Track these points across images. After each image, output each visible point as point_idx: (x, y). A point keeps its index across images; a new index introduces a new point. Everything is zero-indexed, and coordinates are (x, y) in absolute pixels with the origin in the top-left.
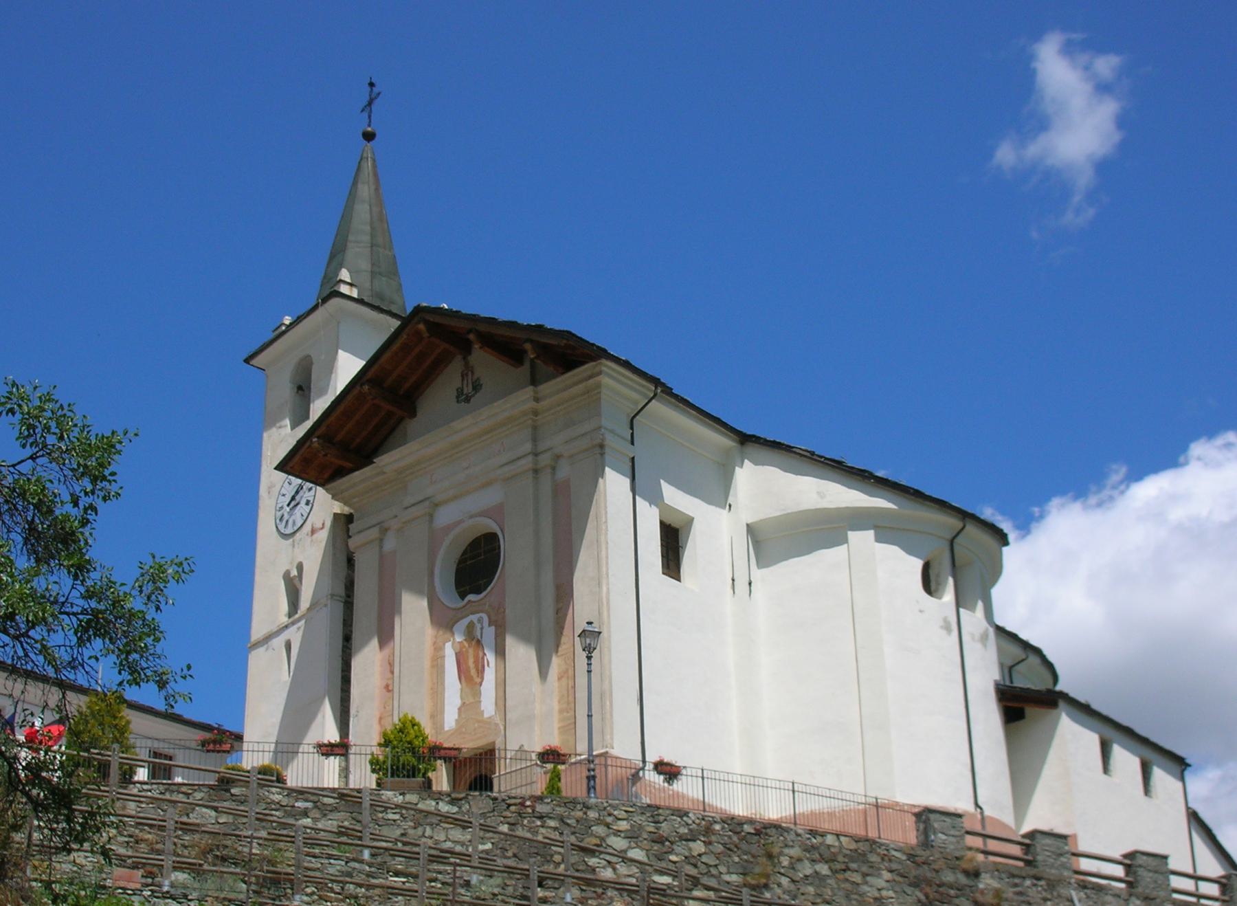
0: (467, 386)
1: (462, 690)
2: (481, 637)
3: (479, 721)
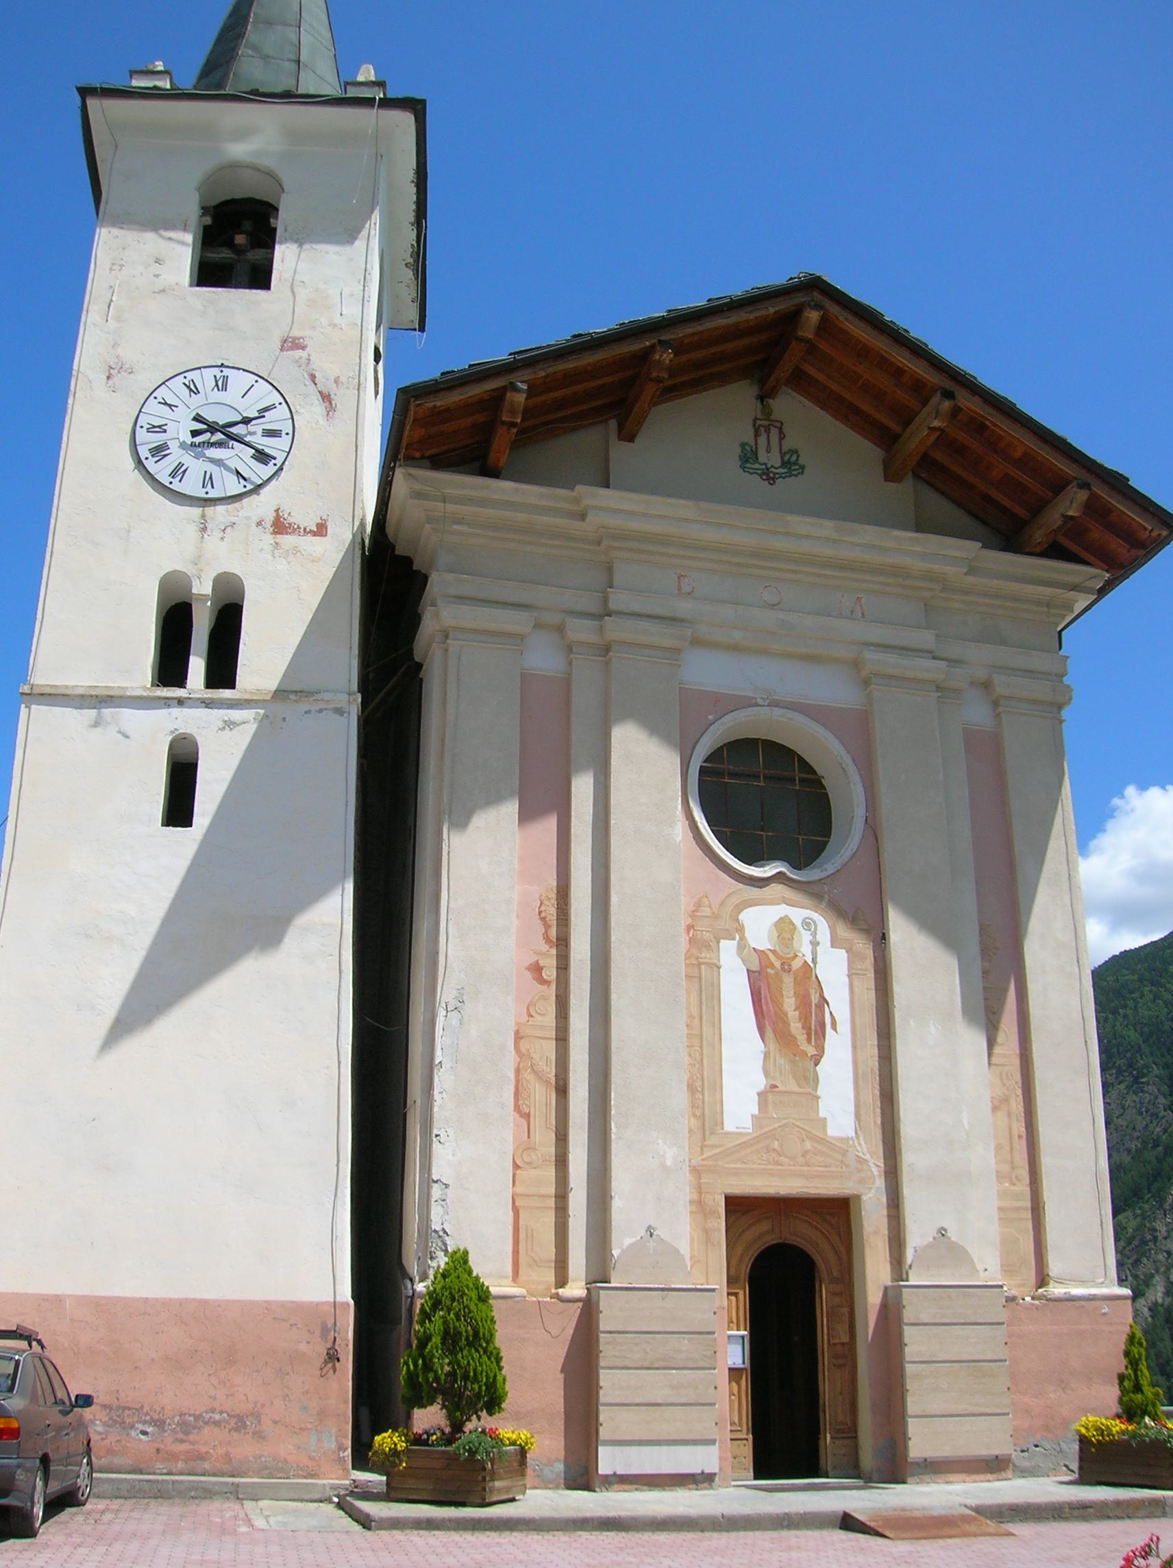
0: (768, 451)
1: (766, 1055)
2: (814, 960)
3: (813, 1138)
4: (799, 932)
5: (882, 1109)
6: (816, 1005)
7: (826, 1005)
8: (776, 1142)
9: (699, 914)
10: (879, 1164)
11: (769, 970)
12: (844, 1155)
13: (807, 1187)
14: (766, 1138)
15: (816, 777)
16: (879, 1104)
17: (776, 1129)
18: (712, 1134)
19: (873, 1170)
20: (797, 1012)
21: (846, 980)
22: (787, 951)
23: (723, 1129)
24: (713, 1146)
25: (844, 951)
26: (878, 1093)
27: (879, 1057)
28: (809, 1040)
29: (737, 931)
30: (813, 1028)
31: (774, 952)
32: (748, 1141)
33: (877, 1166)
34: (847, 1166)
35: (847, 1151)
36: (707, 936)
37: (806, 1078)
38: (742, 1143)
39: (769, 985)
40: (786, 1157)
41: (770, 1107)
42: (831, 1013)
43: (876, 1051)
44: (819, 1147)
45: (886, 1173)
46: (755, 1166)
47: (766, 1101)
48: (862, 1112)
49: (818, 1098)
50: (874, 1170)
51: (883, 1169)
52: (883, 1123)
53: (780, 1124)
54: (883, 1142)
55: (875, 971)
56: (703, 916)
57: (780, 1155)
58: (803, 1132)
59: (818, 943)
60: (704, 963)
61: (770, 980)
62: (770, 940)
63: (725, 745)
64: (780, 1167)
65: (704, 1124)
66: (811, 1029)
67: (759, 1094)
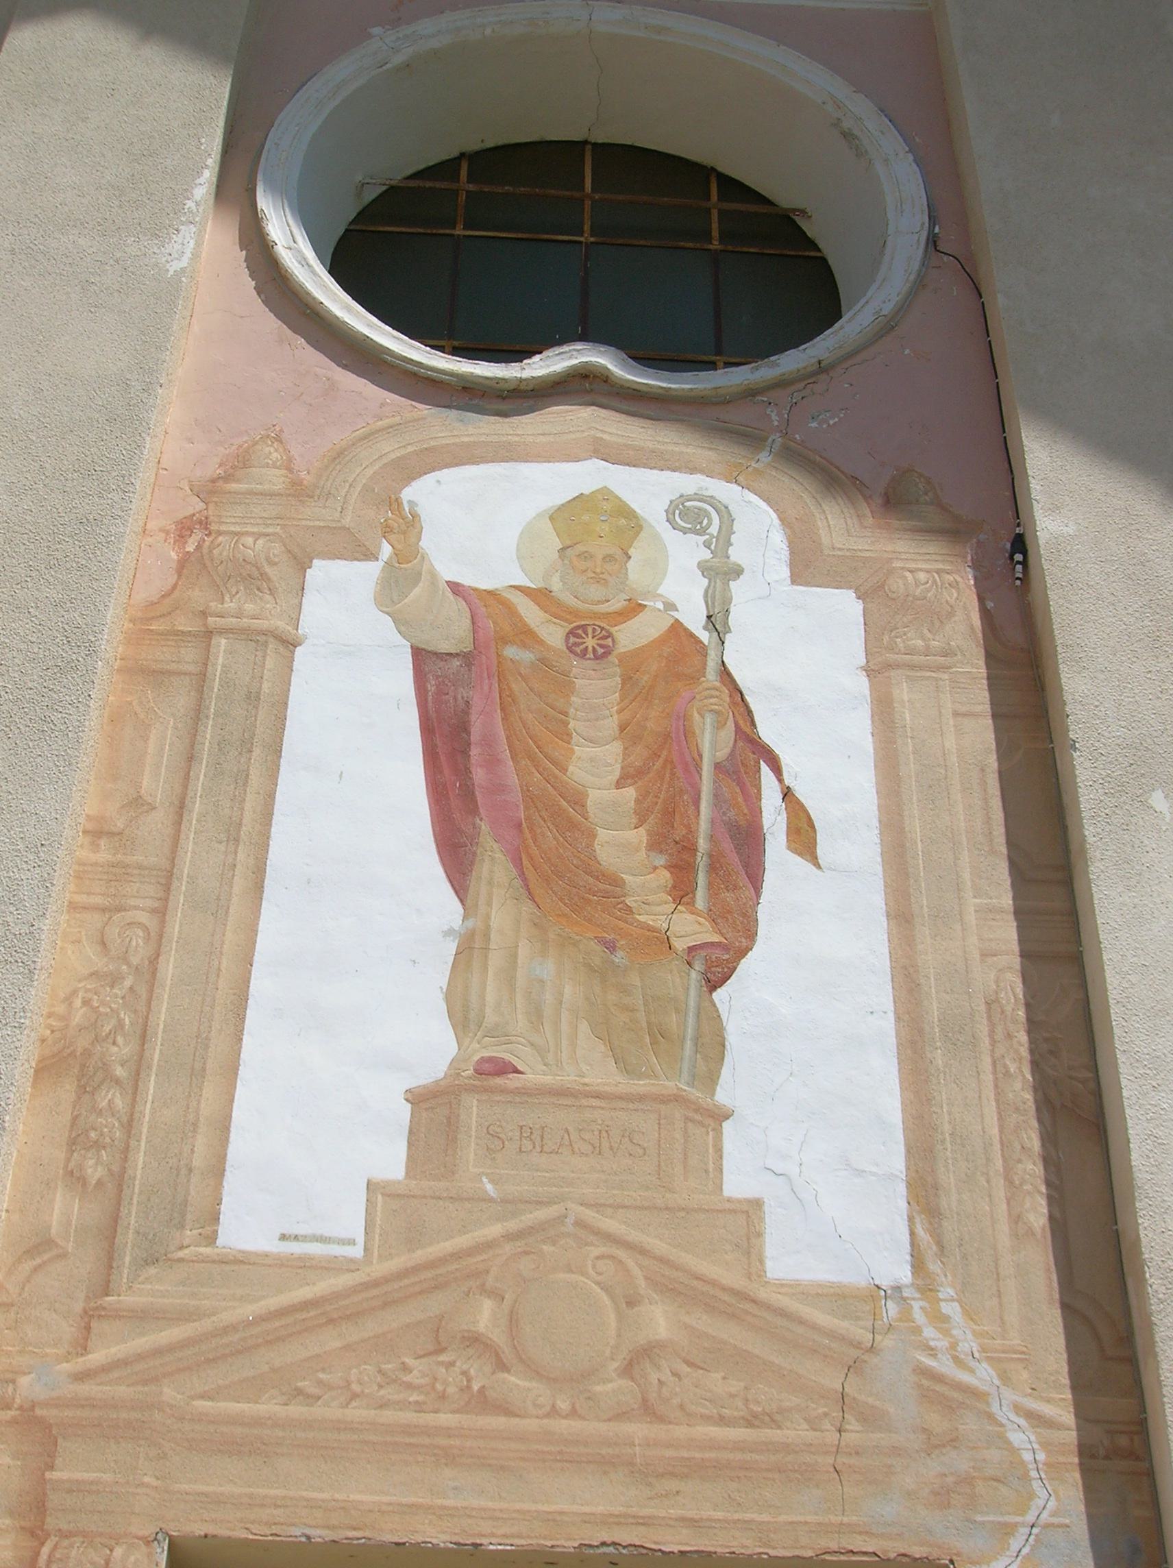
2: (717, 622)
4: (656, 537)
5: (1047, 1161)
6: (718, 766)
7: (765, 769)
8: (487, 1305)
9: (234, 486)
10: (1048, 1410)
11: (510, 652)
12: (853, 1367)
13: (646, 1522)
14: (438, 1286)
15: (818, 254)
16: (1036, 1144)
17: (489, 1245)
18: (153, 1261)
19: (1016, 1438)
20: (630, 793)
21: (861, 685)
22: (595, 592)
23: (212, 1239)
24: (143, 1317)
25: (851, 594)
26: (1028, 1096)
27: (1024, 955)
28: (682, 893)
29: (387, 531)
30: (703, 844)
31: (540, 596)
32: (337, 1296)
33: (1035, 1419)
34: (872, 1419)
35: (872, 1349)
36: (254, 547)
37: (659, 1036)
38: (306, 1305)
39: (507, 704)
40: (535, 1371)
41: (470, 1152)
42: (787, 794)
43: (1008, 933)
44: (731, 1333)
45: (1086, 1452)
46: (357, 1413)
47: (450, 1130)
48: (948, 1178)
49: (721, 1115)
50: (1021, 1438)
51: (1071, 1437)
52: (1059, 1226)
53: (513, 1225)
54: (1066, 1307)
55: (990, 657)
56: (251, 493)
57: (502, 1366)
58: (630, 1263)
59: (737, 572)
60: (223, 631)
61: (517, 687)
62: (524, 557)
63: (462, 155)
64: (498, 1422)
65: (115, 1219)
66: (693, 850)
67: (419, 1099)
